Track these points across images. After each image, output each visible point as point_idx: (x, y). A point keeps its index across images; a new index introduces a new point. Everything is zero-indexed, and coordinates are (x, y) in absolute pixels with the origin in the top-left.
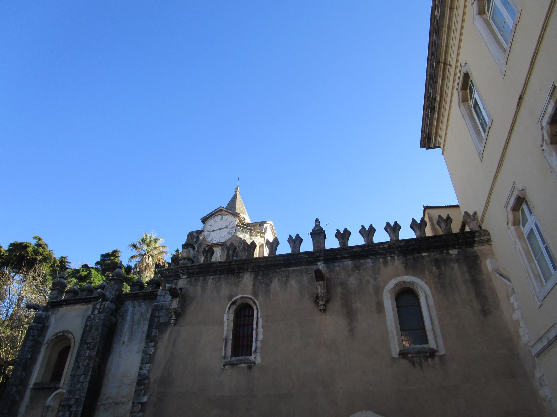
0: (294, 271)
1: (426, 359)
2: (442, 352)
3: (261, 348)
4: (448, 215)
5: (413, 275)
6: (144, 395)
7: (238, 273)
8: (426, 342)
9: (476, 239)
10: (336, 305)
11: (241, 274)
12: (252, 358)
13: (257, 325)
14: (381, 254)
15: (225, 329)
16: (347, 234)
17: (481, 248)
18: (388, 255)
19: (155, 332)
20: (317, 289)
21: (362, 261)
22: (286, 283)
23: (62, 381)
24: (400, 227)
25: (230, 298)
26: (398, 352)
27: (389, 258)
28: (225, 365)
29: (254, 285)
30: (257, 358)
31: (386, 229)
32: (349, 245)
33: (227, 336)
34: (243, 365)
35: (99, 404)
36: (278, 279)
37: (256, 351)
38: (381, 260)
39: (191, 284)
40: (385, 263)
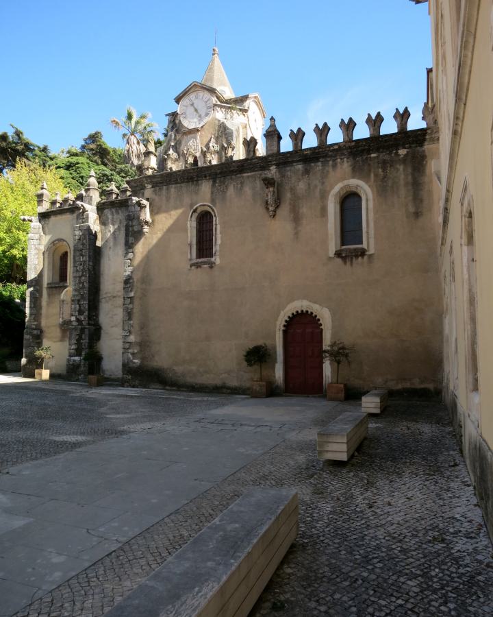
0: (248, 177)
1: (357, 256)
2: (371, 251)
3: (220, 251)
4: (406, 108)
5: (359, 179)
6: (131, 291)
7: (197, 181)
8: (362, 243)
9: (427, 137)
10: (284, 210)
11: (200, 182)
12: (213, 259)
13: (216, 231)
14: (331, 156)
15: (189, 235)
16: (301, 135)
17: (431, 146)
18: (338, 157)
19: (131, 240)
20: (267, 195)
21: (313, 164)
22: (241, 189)
23: (68, 281)
24: (383, 120)
25: (191, 206)
26: (334, 253)
27: (339, 160)
28: (191, 266)
29: (212, 193)
30: (217, 259)
31: (340, 126)
32: (381, 134)
33: (191, 242)
34: (205, 266)
35: (101, 297)
36: (234, 186)
37: (215, 253)
38: (331, 162)
39: (156, 194)
40: (334, 166)
